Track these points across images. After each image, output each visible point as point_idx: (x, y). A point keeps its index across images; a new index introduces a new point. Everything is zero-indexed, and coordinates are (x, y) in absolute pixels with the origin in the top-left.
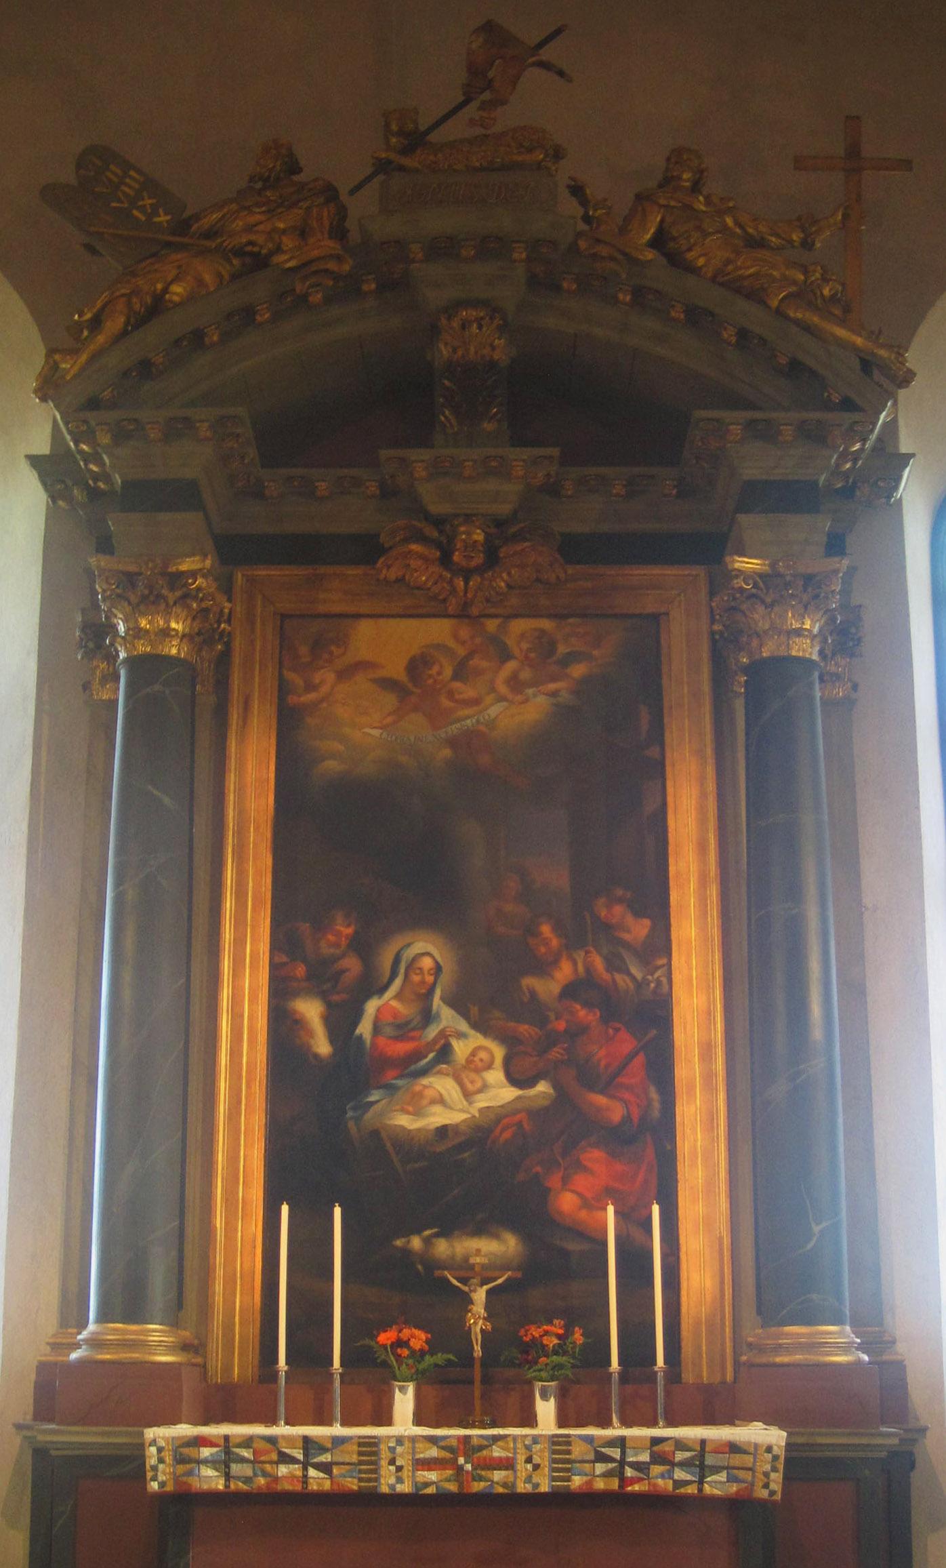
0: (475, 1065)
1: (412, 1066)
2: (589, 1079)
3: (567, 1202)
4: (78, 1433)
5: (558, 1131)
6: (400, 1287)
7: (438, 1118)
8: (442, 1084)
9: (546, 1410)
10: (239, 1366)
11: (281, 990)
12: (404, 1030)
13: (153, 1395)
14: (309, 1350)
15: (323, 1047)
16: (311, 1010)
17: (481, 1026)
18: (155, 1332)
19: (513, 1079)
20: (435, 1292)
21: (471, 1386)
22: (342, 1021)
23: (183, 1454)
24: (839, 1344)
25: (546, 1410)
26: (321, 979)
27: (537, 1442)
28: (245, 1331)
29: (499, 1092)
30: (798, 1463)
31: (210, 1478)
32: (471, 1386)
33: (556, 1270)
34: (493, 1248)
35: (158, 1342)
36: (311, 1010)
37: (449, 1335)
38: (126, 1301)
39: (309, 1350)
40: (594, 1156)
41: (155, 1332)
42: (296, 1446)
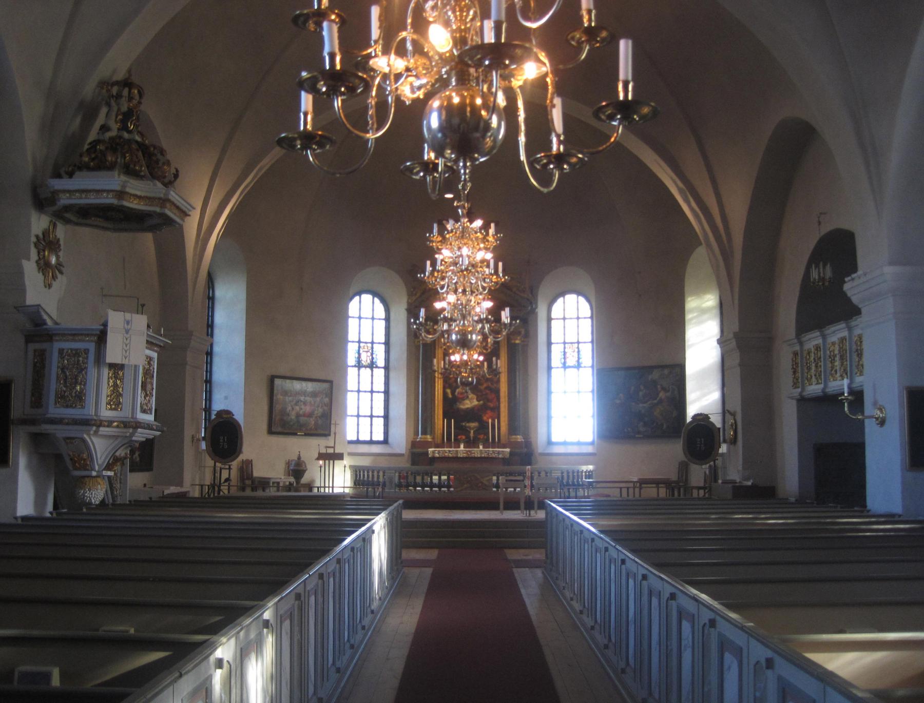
0: (472, 399)
1: (463, 399)
2: (489, 400)
3: (485, 418)
4: (194, 516)
5: (483, 408)
6: (461, 430)
7: (467, 406)
8: (467, 401)
9: (481, 447)
10: (439, 441)
11: (444, 388)
12: (462, 393)
13: (427, 445)
14: (449, 439)
15: (450, 396)
16: (449, 391)
17: (473, 393)
18: (428, 436)
19: (478, 400)
20: (465, 431)
21: (470, 443)
22: (453, 393)
23: (434, 452)
24: (520, 438)
25: (481, 447)
26: (450, 387)
27: (480, 450)
28: (440, 432)
29: (475, 403)
30: (511, 453)
31: (437, 455)
32: (470, 443)
33: (483, 427)
34: (473, 425)
35: (429, 438)
36: (449, 391)
37: (468, 437)
38: (424, 432)
39: (449, 439)
40: (489, 412)
41: (428, 436)
42: (448, 451)
